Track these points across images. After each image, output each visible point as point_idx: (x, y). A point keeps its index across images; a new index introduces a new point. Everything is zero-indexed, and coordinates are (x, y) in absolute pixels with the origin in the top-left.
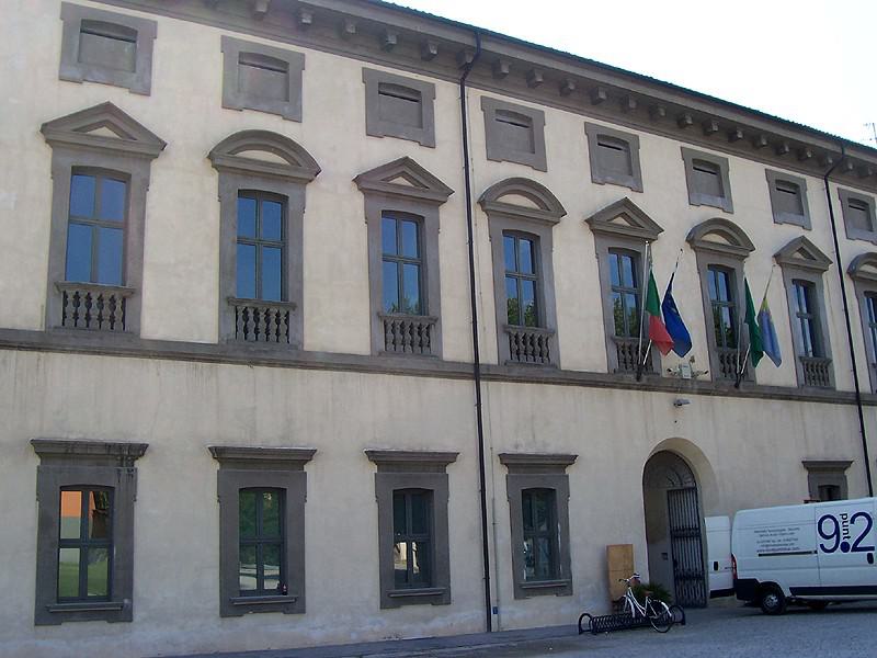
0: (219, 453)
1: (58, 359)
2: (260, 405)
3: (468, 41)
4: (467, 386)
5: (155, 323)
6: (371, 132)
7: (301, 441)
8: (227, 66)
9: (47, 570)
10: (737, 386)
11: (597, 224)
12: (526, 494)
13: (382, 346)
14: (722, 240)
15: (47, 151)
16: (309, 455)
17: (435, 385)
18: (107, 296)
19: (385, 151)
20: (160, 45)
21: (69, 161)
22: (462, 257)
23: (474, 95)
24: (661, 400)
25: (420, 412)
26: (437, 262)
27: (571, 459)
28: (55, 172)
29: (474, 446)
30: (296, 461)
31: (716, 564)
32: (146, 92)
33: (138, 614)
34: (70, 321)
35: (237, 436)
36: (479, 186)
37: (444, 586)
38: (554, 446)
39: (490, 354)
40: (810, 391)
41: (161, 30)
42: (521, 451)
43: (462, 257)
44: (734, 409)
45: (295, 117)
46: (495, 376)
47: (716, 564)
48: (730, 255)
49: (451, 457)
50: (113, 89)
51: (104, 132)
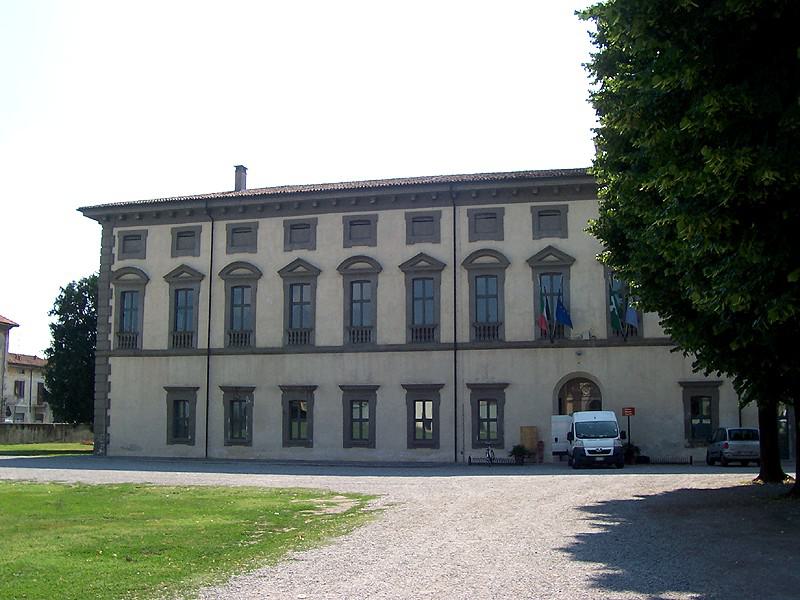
0: (681, 384)
1: (288, 357)
2: (358, 367)
3: (446, 189)
5: (321, 340)
9: (412, 429)
10: (552, 342)
13: (474, 337)
15: (281, 280)
16: (377, 387)
17: (436, 355)
18: (491, 326)
19: (413, 251)
21: (288, 283)
22: (269, 300)
23: (463, 210)
24: (568, 353)
31: (556, 440)
33: (315, 445)
34: (415, 339)
35: (350, 381)
36: (462, 255)
40: (174, 352)
41: (443, 213)
42: (479, 382)
43: (269, 300)
44: (623, 355)
46: (220, 352)
47: (556, 440)
48: (431, 271)
49: (442, 386)
51: (423, 263)
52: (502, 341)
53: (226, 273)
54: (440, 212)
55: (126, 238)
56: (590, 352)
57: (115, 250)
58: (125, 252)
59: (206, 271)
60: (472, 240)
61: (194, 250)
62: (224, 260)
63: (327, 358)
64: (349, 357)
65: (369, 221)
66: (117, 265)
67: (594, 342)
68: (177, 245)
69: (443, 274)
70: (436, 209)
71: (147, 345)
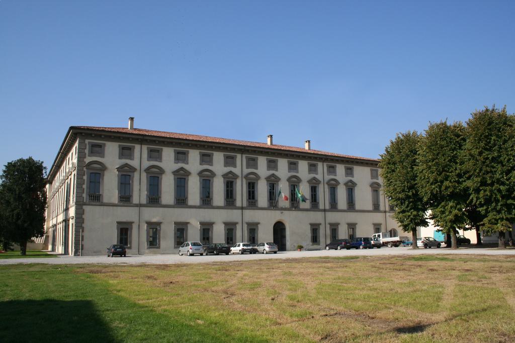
2: (207, 215)
4: (240, 211)
6: (225, 166)
7: (212, 221)
8: (148, 152)
11: (346, 184)
12: (333, 229)
14: (158, 170)
16: (259, 223)
17: (235, 211)
20: (106, 148)
23: (244, 156)
24: (278, 212)
25: (233, 215)
26: (236, 189)
27: (259, 223)
28: (175, 179)
29: (138, 221)
30: (211, 224)
32: (188, 164)
37: (361, 240)
38: (256, 221)
39: (245, 204)
44: (294, 213)
45: (212, 165)
46: (329, 211)
48: (184, 175)
49: (320, 224)
50: (184, 164)
52: (212, 206)
53: (147, 170)
54: (236, 156)
55: (93, 146)
56: (286, 212)
57: (87, 151)
58: (92, 153)
59: (138, 168)
60: (247, 168)
61: (131, 157)
62: (146, 164)
63: (305, 213)
64: (312, 213)
65: (101, 146)
66: (88, 160)
67: (285, 209)
68: (122, 154)
69: (237, 180)
70: (187, 150)
71: (105, 200)
